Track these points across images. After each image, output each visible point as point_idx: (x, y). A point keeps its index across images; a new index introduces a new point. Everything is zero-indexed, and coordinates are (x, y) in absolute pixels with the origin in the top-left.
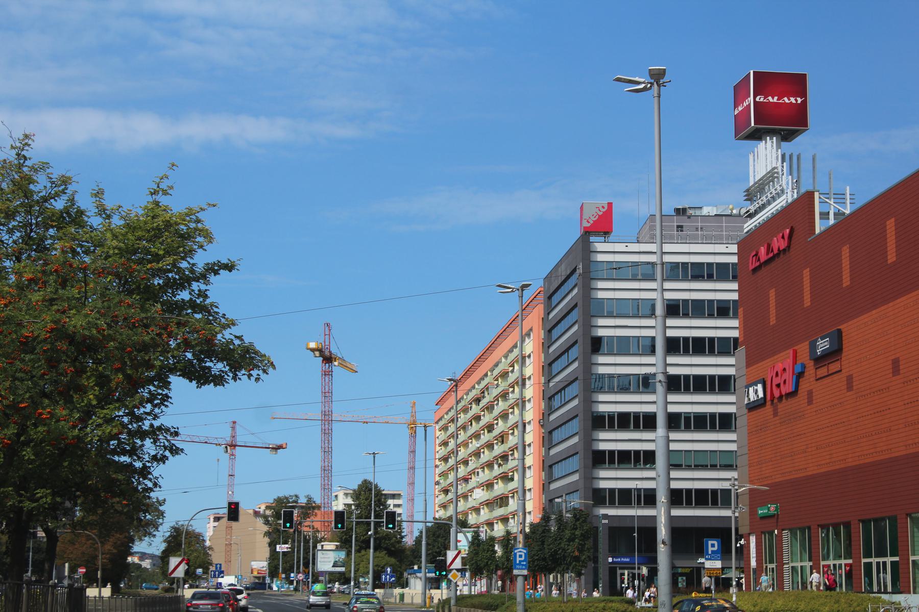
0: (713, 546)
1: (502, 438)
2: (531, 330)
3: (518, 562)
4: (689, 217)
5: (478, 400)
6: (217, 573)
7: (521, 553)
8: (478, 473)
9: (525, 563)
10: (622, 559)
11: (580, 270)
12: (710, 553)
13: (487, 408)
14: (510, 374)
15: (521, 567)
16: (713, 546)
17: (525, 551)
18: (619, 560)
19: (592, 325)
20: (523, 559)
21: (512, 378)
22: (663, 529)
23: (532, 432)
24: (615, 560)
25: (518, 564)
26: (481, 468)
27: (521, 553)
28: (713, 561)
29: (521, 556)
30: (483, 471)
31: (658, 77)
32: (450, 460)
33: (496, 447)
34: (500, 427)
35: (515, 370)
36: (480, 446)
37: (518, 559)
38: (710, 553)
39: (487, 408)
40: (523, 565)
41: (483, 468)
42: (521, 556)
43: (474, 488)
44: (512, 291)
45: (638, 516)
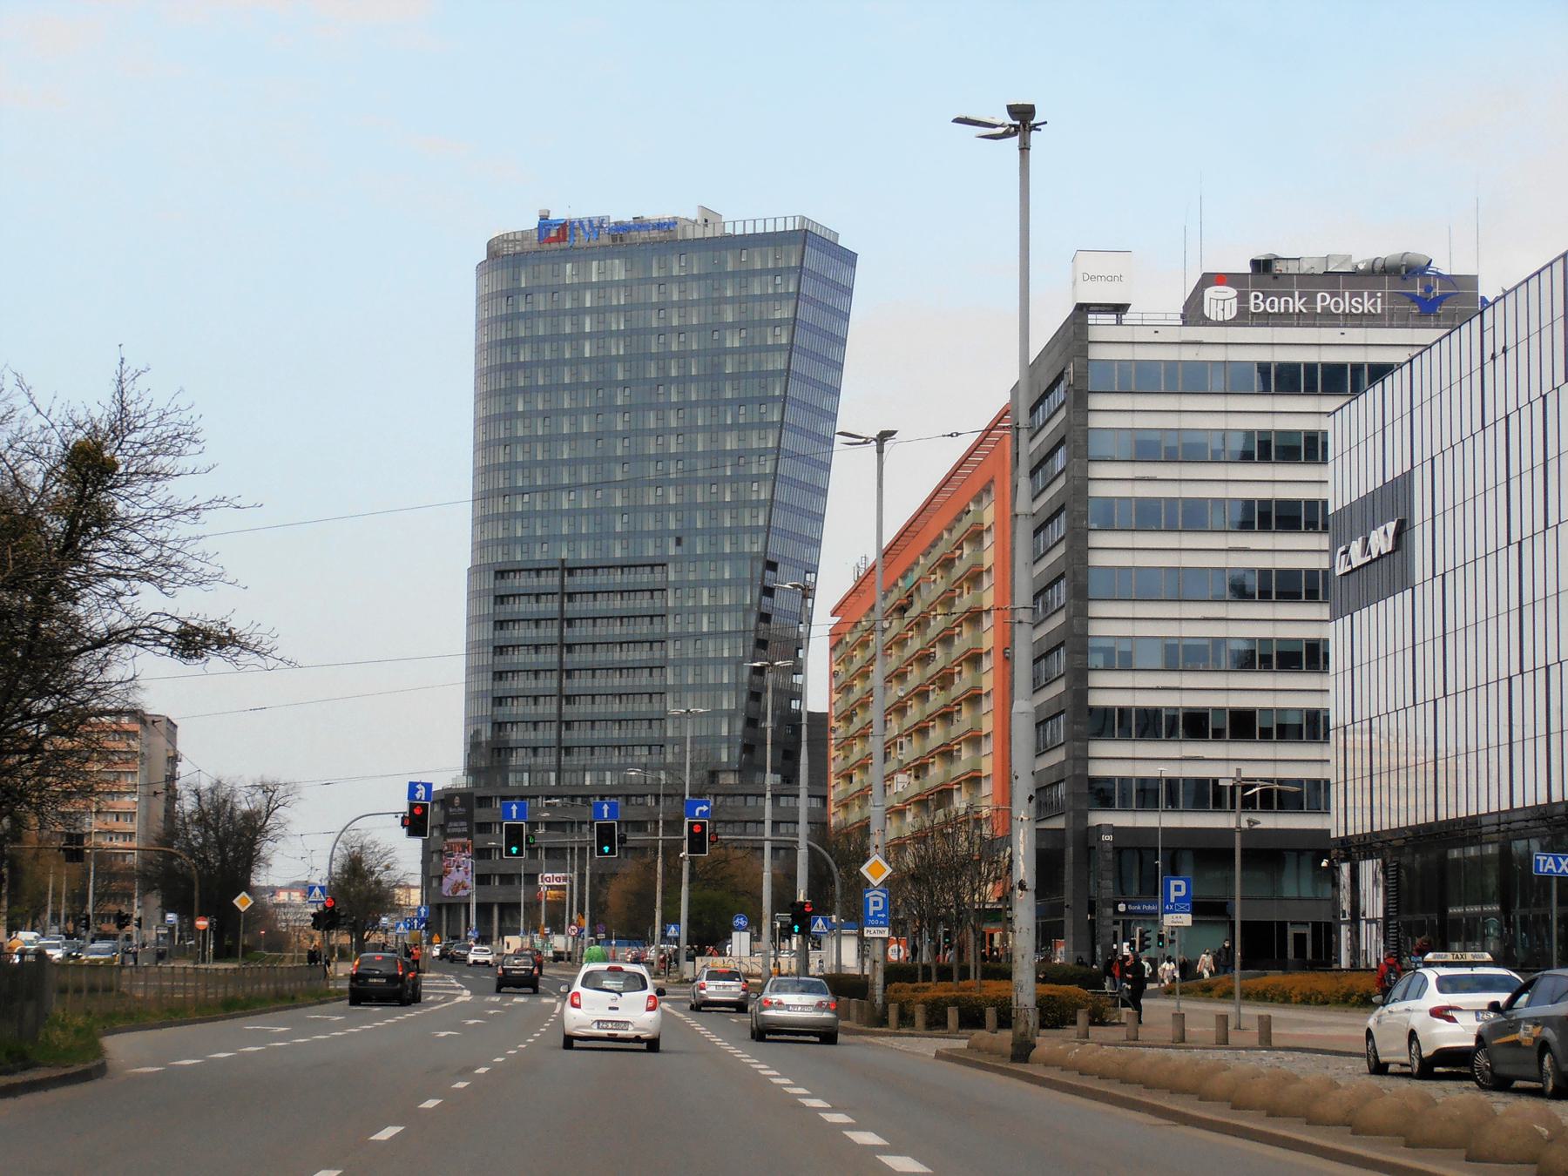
0: (1178, 888)
1: (945, 679)
2: (992, 481)
3: (871, 914)
4: (1276, 277)
5: (902, 609)
6: (416, 921)
7: (876, 899)
8: (901, 743)
9: (883, 915)
10: (1144, 907)
11: (1070, 377)
12: (1172, 900)
13: (918, 624)
14: (957, 562)
15: (877, 922)
16: (1178, 888)
17: (884, 895)
18: (1139, 908)
19: (1090, 476)
20: (880, 908)
21: (960, 568)
22: (1021, 863)
23: (992, 671)
24: (1130, 907)
25: (871, 918)
26: (907, 736)
27: (876, 899)
28: (1179, 915)
29: (876, 903)
30: (910, 741)
31: (1023, 117)
32: (855, 719)
33: (932, 696)
34: (940, 657)
35: (964, 556)
36: (905, 696)
37: (872, 909)
38: (1172, 900)
39: (918, 624)
40: (880, 919)
41: (910, 735)
42: (876, 903)
43: (894, 772)
44: (865, 443)
45: (1163, 829)
